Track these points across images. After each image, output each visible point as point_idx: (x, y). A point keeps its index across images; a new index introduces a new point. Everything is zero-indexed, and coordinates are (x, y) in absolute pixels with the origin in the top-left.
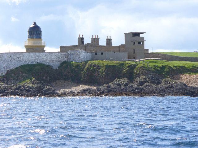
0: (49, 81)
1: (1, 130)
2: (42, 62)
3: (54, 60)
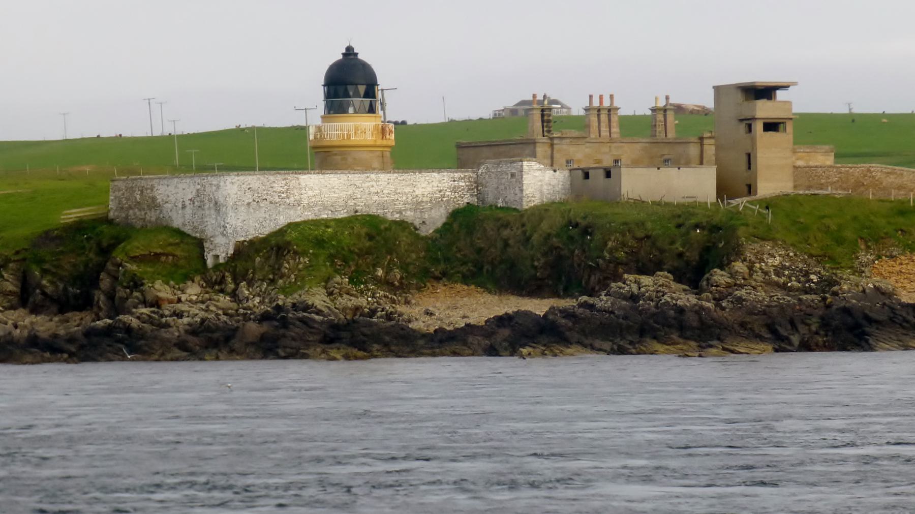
0: (401, 283)
1: (913, 491)
2: (373, 211)
3: (425, 199)
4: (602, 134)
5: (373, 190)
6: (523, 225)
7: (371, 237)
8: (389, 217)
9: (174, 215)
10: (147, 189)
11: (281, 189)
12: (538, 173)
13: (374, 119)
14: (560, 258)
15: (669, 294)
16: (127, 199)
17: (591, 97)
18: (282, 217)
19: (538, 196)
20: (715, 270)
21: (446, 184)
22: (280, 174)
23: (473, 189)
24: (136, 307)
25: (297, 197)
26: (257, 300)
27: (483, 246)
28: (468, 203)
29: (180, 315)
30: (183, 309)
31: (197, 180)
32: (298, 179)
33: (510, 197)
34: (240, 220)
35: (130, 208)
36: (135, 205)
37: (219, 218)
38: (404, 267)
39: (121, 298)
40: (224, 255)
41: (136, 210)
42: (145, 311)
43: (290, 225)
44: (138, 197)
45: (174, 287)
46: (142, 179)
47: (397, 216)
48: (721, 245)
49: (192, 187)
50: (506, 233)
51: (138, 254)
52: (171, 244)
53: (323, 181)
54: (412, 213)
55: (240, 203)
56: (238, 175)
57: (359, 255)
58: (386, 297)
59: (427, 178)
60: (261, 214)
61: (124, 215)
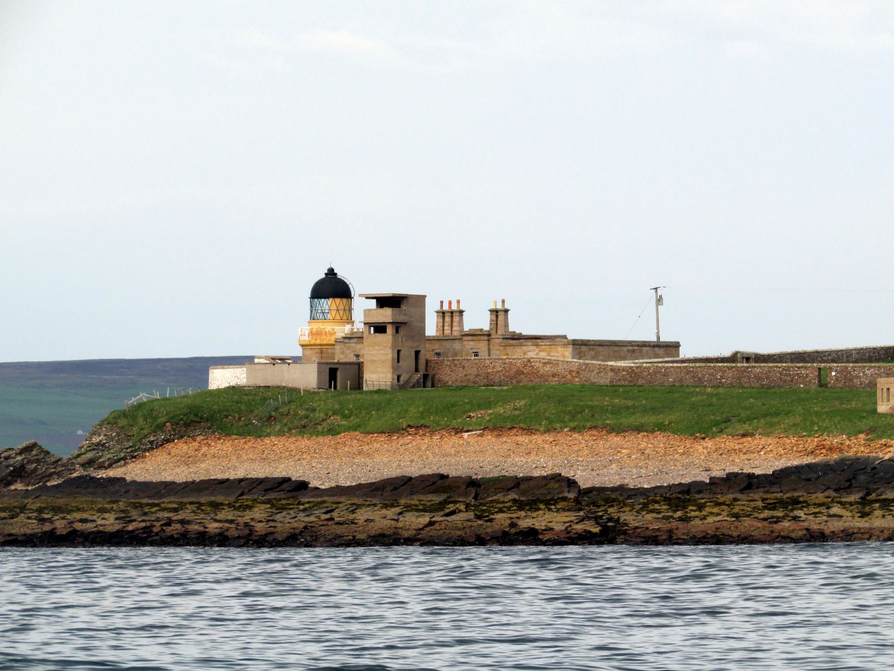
17: (442, 302)
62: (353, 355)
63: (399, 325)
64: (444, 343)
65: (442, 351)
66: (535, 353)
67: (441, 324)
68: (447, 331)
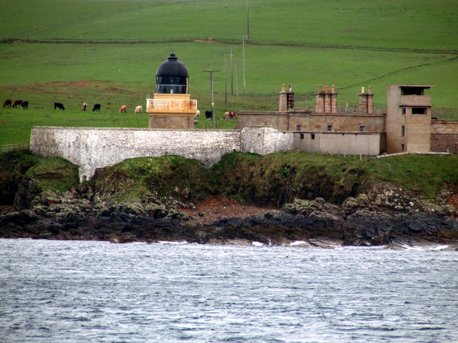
2: (177, 153)
3: (208, 147)
4: (326, 109)
5: (177, 140)
6: (261, 165)
7: (173, 168)
8: (186, 156)
9: (64, 151)
10: (50, 134)
11: (123, 139)
12: (273, 134)
13: (184, 97)
14: (279, 185)
15: (315, 211)
16: (40, 140)
18: (122, 155)
19: (273, 147)
20: (350, 197)
21: (222, 138)
22: (123, 130)
23: (238, 142)
24: (36, 205)
25: (132, 144)
26: (104, 203)
27: (239, 175)
28: (234, 150)
29: (58, 210)
30: (61, 207)
31: (77, 131)
32: (133, 133)
33: (257, 148)
34: (99, 156)
35: (41, 145)
36: (44, 143)
37: (87, 154)
38: (192, 185)
39: (29, 199)
40: (89, 176)
41: (44, 146)
42: (40, 207)
43: (126, 160)
44: (46, 138)
45: (59, 194)
46: (48, 128)
47: (191, 156)
48: (362, 183)
49: (74, 135)
50: (252, 169)
51: (40, 174)
52: (60, 168)
53: (147, 135)
54: (200, 155)
55: (99, 146)
56: (99, 130)
57: (165, 179)
58: (179, 204)
59: (210, 134)
60: (111, 153)
61: (37, 149)
62: (296, 125)
63: (404, 108)
64: (368, 119)
65: (367, 125)
66: (443, 129)
67: (323, 103)
68: (328, 109)
